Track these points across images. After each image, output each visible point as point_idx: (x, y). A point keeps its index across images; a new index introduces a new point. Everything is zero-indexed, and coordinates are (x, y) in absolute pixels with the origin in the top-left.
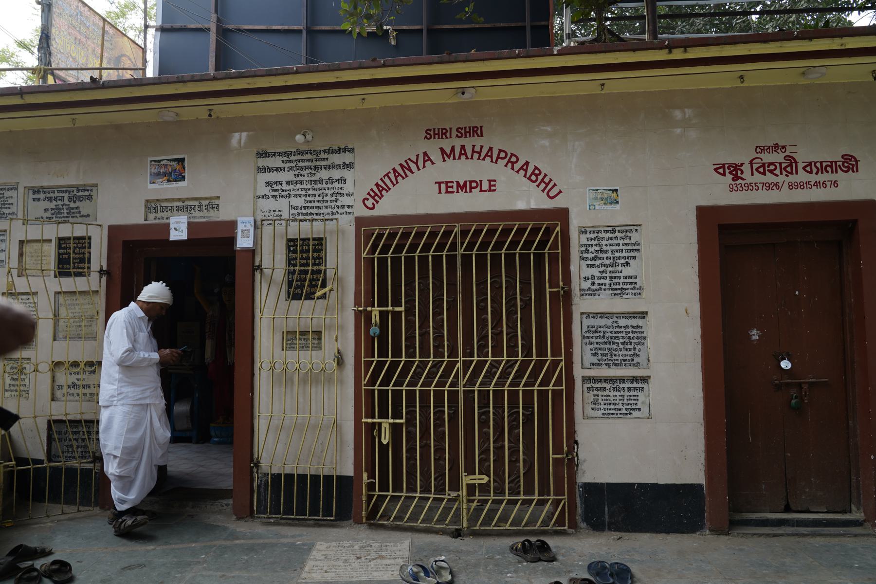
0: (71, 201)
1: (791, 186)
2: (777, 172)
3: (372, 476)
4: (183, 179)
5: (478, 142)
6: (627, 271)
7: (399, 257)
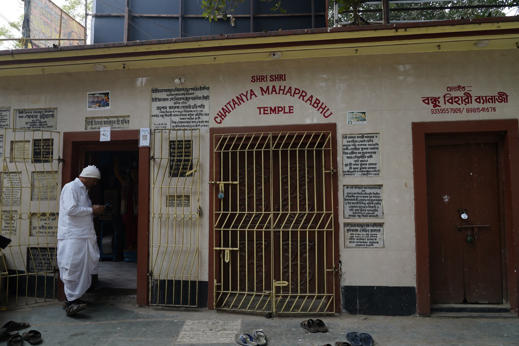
0: (42, 118)
1: (468, 111)
2: (460, 102)
3: (219, 281)
5: (283, 84)
6: (371, 161)
7: (236, 152)
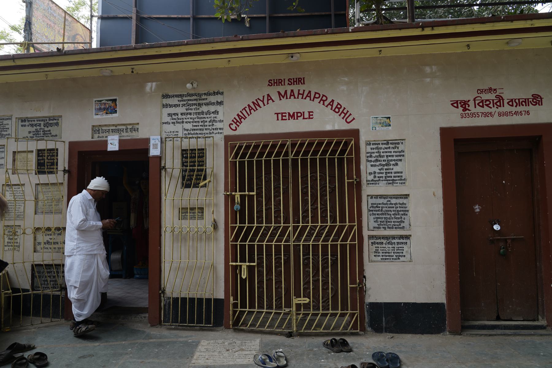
0: (46, 126)
1: (500, 115)
2: (491, 105)
3: (236, 298)
4: (116, 112)
5: (301, 87)
6: (396, 169)
7: (252, 160)
